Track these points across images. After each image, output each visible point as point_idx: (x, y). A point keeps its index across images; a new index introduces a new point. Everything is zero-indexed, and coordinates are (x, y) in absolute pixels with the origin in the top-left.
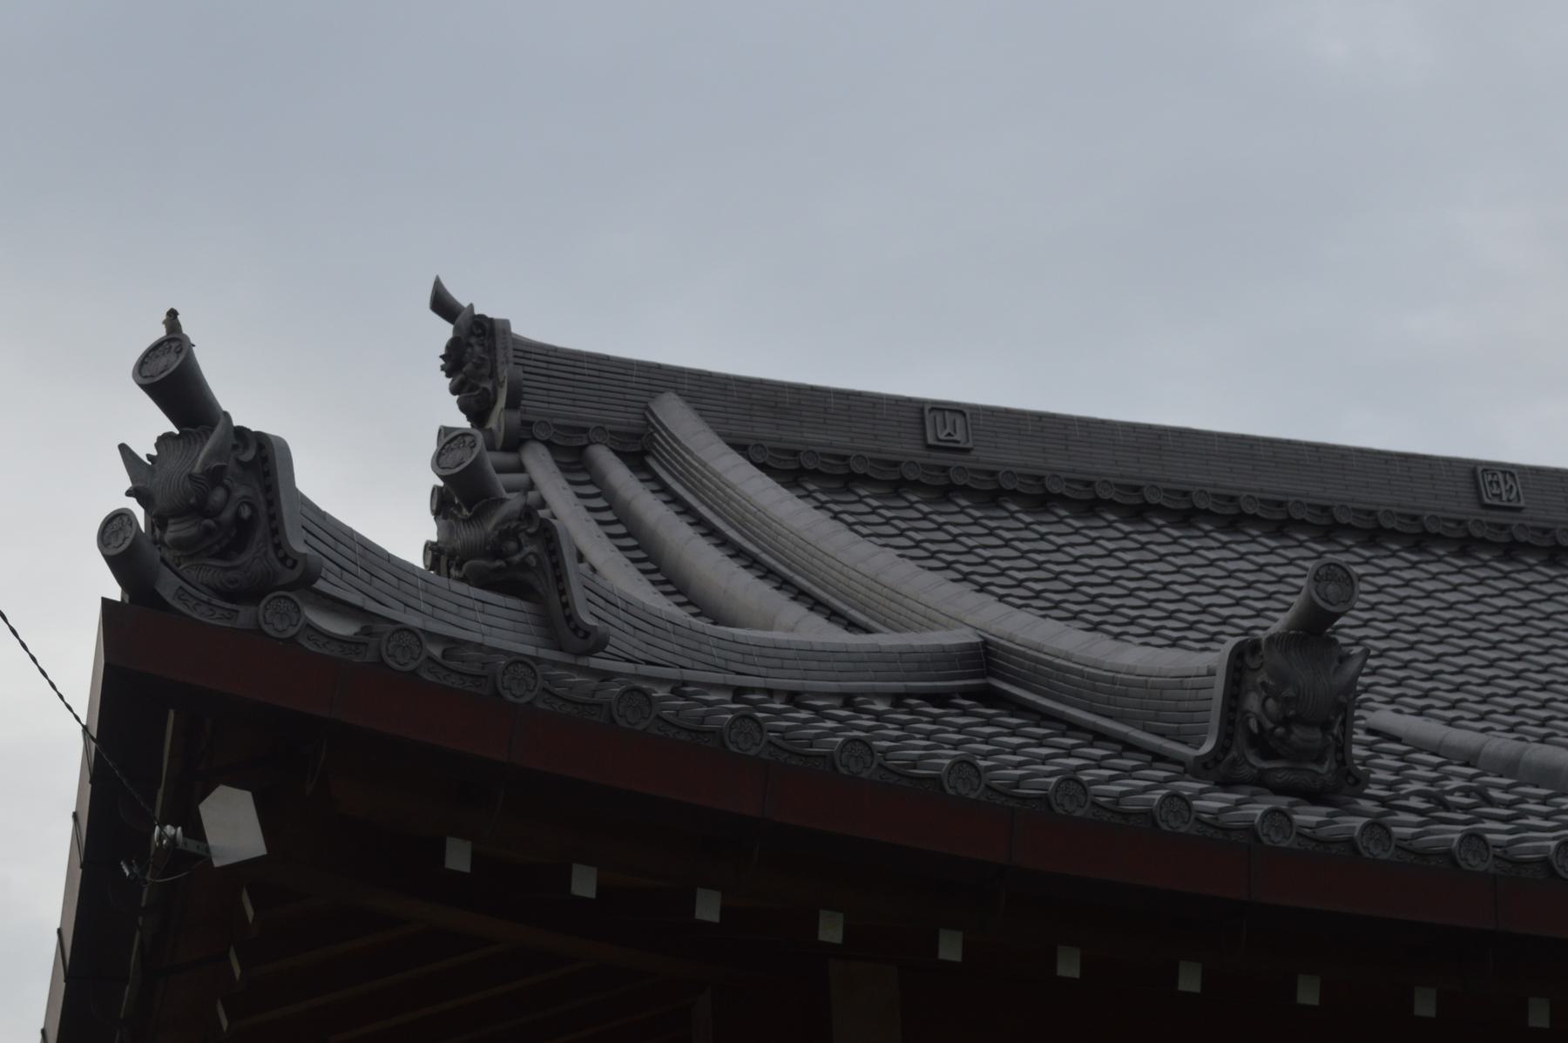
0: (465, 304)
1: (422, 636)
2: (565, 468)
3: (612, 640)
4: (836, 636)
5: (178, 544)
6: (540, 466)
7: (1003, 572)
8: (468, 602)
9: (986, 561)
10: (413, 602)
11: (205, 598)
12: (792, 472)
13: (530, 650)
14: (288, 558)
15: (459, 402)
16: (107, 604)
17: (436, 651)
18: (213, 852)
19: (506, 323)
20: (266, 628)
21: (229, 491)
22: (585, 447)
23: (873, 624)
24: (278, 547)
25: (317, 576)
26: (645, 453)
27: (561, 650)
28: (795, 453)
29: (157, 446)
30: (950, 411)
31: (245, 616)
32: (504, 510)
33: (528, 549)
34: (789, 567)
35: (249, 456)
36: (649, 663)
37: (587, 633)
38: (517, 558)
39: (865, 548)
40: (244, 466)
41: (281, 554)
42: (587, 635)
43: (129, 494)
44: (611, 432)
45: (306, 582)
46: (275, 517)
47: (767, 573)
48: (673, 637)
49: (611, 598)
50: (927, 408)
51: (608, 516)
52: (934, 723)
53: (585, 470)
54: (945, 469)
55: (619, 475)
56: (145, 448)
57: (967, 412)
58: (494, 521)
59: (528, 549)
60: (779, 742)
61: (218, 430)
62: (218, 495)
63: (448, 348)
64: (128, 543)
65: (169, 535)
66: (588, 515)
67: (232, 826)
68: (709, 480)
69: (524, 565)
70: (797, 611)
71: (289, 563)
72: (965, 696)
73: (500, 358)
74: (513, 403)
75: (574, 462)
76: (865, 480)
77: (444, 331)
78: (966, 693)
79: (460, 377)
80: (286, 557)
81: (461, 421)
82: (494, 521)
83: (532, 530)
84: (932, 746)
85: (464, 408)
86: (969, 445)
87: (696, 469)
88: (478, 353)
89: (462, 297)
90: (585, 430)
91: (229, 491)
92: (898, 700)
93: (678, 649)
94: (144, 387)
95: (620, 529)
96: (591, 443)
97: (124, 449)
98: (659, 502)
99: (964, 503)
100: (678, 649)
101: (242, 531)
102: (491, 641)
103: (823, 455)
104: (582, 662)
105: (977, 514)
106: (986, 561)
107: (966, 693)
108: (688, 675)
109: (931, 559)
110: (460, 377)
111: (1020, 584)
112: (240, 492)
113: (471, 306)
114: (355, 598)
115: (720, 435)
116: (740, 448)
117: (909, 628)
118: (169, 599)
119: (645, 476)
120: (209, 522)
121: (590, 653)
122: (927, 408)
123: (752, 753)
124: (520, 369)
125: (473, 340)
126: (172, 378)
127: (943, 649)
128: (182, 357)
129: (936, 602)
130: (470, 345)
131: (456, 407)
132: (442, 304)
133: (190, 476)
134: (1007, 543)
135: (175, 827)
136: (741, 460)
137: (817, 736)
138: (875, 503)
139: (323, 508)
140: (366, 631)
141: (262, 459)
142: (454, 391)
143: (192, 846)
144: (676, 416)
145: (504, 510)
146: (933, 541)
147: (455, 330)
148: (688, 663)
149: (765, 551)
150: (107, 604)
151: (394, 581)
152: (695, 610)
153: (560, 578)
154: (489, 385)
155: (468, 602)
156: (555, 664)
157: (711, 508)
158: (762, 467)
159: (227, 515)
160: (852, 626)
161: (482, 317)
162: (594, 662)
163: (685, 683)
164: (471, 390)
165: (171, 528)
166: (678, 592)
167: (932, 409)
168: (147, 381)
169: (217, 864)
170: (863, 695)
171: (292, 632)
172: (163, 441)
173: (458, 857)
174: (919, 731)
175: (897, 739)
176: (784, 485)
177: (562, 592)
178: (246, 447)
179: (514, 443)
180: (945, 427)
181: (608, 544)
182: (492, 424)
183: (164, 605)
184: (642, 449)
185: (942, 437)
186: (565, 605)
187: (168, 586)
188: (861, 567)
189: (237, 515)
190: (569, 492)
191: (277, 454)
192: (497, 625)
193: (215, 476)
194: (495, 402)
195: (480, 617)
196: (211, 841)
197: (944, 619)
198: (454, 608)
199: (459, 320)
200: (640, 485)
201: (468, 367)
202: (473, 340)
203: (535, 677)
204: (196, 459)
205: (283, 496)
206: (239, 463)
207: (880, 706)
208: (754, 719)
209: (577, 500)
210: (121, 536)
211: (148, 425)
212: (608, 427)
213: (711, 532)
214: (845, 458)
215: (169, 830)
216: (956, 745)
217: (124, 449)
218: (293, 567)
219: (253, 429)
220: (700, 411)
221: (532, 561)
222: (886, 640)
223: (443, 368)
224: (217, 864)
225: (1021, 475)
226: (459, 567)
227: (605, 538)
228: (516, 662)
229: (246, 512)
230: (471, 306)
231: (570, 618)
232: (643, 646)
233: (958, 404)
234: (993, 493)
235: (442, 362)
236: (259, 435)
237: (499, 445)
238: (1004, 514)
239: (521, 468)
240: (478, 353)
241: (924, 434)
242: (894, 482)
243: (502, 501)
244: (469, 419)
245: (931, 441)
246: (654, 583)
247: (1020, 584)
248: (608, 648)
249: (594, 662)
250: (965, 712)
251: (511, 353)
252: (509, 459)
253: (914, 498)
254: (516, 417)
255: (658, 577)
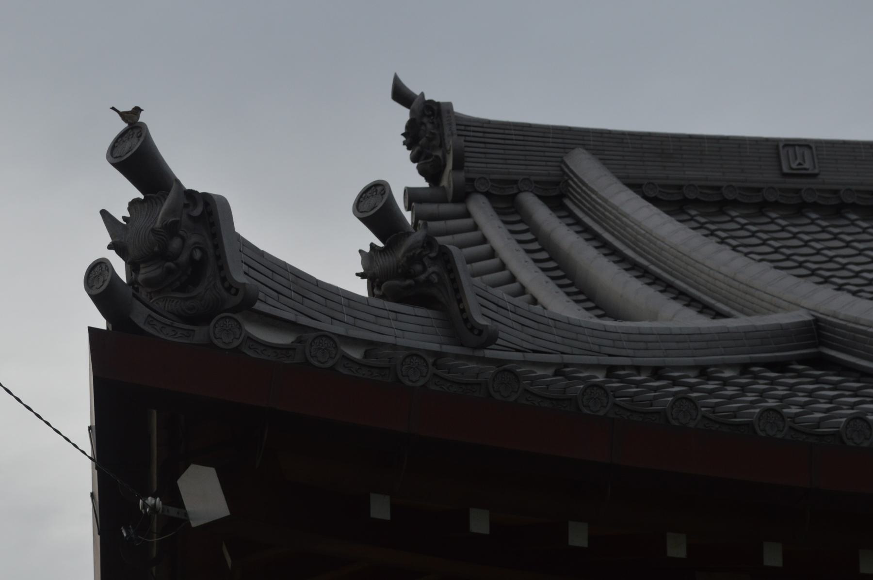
0: (417, 92)
1: (336, 339)
2: (500, 212)
3: (501, 334)
4: (704, 322)
5: (148, 282)
6: (481, 211)
7: (843, 267)
8: (384, 313)
9: (831, 259)
10: (339, 316)
11: (168, 322)
12: (675, 201)
13: (435, 347)
14: (232, 288)
15: (418, 167)
16: (93, 332)
17: (357, 354)
18: (191, 516)
19: (449, 105)
20: (215, 341)
21: (184, 240)
22: (516, 194)
23: (733, 312)
24: (224, 280)
25: (256, 299)
26: (562, 196)
27: (462, 345)
28: (680, 187)
29: (129, 209)
30: (800, 146)
31: (200, 334)
32: (410, 241)
33: (431, 270)
34: (671, 274)
35: (197, 212)
36: (535, 351)
37: (480, 331)
38: (423, 277)
39: (726, 253)
40: (194, 219)
41: (226, 285)
42: (481, 332)
43: (110, 247)
44: (536, 182)
45: (247, 305)
46: (220, 256)
47: (654, 280)
48: (555, 331)
49: (501, 303)
50: (781, 145)
51: (535, 246)
52: (856, 396)
53: (517, 212)
54: (798, 191)
55: (542, 214)
56: (120, 212)
57: (813, 146)
58: (402, 250)
59: (431, 270)
60: (711, 416)
61: (172, 194)
62: (176, 244)
63: (407, 127)
64: (106, 284)
65: (141, 277)
66: (518, 246)
67: (203, 495)
68: (610, 213)
69: (428, 282)
70: (676, 306)
71: (233, 291)
72: (800, 363)
73: (447, 132)
74: (458, 165)
75: (507, 206)
76: (735, 204)
77: (403, 115)
78: (802, 360)
79: (417, 148)
80: (231, 287)
81: (421, 182)
82: (402, 250)
83: (433, 255)
84: (748, 401)
85: (422, 172)
86: (816, 171)
87: (600, 205)
88: (429, 128)
89: (415, 87)
90: (515, 182)
91: (184, 240)
92: (744, 368)
93: (558, 339)
94: (115, 165)
95: (544, 255)
96: (520, 192)
97: (104, 214)
98: (572, 232)
99: (814, 216)
100: (558, 339)
101: (197, 269)
102: (401, 342)
103: (701, 187)
104: (479, 353)
105: (824, 223)
106: (831, 259)
107: (802, 360)
108: (567, 359)
109: (782, 261)
110: (417, 148)
111: (857, 275)
112: (193, 239)
113: (422, 94)
114: (289, 315)
115: (619, 178)
116: (636, 187)
117: (756, 312)
118: (141, 325)
119: (564, 214)
120: (171, 264)
121: (484, 346)
122: (781, 145)
123: (601, 413)
124: (463, 138)
125: (425, 120)
126: (136, 156)
127: (781, 327)
128: (142, 139)
129: (781, 293)
130: (423, 124)
131: (416, 171)
132: (401, 95)
133: (153, 230)
134: (848, 245)
135: (155, 497)
136: (634, 195)
137: (740, 408)
138: (743, 221)
139: (261, 248)
140: (299, 341)
141: (209, 212)
142: (414, 159)
143: (173, 512)
144: (586, 167)
145: (410, 241)
146: (788, 247)
147: (412, 113)
148: (568, 350)
149: (652, 263)
150: (93, 332)
151: (322, 300)
152: (600, 312)
153: (458, 290)
154: (439, 153)
155: (384, 313)
156: (457, 357)
157: (613, 234)
158: (655, 201)
159: (184, 258)
160: (705, 309)
161: (431, 101)
162: (488, 353)
163: (566, 365)
164: (426, 158)
165: (142, 271)
166: (588, 300)
167: (785, 146)
168: (117, 161)
169: (194, 524)
170: (715, 366)
171: (236, 343)
172: (134, 204)
173: (380, 509)
174: (823, 397)
175: (828, 410)
176: (668, 213)
177: (460, 301)
178: (195, 205)
179: (461, 196)
180: (796, 159)
181: (533, 267)
182: (444, 183)
183: (142, 332)
184: (560, 194)
185: (794, 166)
186: (463, 311)
187: (139, 315)
188: (723, 269)
189: (191, 257)
190: (504, 230)
191: (219, 209)
192: (413, 330)
193: (171, 229)
194: (445, 166)
195: (393, 324)
196: (188, 508)
197: (785, 304)
198: (372, 319)
199: (414, 105)
200: (558, 220)
201: (423, 141)
202: (425, 120)
203: (427, 365)
204: (156, 219)
205: (225, 241)
206: (190, 217)
207: (727, 374)
208: (690, 400)
209: (510, 236)
210: (101, 279)
211: (121, 194)
212: (533, 178)
213: (612, 252)
214: (719, 188)
215: (150, 500)
216: (852, 406)
217: (104, 214)
218: (236, 294)
219: (200, 192)
220: (604, 161)
221: (435, 278)
222: (738, 322)
223: (404, 143)
224: (194, 524)
225: (858, 191)
226: (379, 287)
227: (531, 262)
228: (852, 419)
229: (198, 255)
230: (422, 94)
231: (467, 320)
232: (531, 339)
233: (805, 140)
234: (836, 207)
235: (403, 139)
236: (205, 195)
237: (450, 198)
238: (847, 222)
239: (467, 215)
240: (429, 128)
241: (780, 165)
242: (759, 203)
243: (409, 234)
244: (427, 180)
245: (785, 170)
246: (568, 294)
247: (857, 275)
248: (499, 341)
249: (488, 353)
250: (799, 374)
251: (454, 127)
252: (458, 208)
253: (774, 215)
254: (461, 176)
255: (573, 289)
